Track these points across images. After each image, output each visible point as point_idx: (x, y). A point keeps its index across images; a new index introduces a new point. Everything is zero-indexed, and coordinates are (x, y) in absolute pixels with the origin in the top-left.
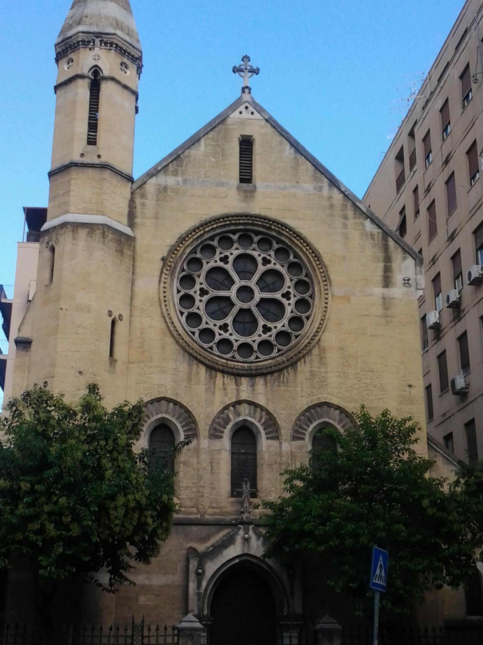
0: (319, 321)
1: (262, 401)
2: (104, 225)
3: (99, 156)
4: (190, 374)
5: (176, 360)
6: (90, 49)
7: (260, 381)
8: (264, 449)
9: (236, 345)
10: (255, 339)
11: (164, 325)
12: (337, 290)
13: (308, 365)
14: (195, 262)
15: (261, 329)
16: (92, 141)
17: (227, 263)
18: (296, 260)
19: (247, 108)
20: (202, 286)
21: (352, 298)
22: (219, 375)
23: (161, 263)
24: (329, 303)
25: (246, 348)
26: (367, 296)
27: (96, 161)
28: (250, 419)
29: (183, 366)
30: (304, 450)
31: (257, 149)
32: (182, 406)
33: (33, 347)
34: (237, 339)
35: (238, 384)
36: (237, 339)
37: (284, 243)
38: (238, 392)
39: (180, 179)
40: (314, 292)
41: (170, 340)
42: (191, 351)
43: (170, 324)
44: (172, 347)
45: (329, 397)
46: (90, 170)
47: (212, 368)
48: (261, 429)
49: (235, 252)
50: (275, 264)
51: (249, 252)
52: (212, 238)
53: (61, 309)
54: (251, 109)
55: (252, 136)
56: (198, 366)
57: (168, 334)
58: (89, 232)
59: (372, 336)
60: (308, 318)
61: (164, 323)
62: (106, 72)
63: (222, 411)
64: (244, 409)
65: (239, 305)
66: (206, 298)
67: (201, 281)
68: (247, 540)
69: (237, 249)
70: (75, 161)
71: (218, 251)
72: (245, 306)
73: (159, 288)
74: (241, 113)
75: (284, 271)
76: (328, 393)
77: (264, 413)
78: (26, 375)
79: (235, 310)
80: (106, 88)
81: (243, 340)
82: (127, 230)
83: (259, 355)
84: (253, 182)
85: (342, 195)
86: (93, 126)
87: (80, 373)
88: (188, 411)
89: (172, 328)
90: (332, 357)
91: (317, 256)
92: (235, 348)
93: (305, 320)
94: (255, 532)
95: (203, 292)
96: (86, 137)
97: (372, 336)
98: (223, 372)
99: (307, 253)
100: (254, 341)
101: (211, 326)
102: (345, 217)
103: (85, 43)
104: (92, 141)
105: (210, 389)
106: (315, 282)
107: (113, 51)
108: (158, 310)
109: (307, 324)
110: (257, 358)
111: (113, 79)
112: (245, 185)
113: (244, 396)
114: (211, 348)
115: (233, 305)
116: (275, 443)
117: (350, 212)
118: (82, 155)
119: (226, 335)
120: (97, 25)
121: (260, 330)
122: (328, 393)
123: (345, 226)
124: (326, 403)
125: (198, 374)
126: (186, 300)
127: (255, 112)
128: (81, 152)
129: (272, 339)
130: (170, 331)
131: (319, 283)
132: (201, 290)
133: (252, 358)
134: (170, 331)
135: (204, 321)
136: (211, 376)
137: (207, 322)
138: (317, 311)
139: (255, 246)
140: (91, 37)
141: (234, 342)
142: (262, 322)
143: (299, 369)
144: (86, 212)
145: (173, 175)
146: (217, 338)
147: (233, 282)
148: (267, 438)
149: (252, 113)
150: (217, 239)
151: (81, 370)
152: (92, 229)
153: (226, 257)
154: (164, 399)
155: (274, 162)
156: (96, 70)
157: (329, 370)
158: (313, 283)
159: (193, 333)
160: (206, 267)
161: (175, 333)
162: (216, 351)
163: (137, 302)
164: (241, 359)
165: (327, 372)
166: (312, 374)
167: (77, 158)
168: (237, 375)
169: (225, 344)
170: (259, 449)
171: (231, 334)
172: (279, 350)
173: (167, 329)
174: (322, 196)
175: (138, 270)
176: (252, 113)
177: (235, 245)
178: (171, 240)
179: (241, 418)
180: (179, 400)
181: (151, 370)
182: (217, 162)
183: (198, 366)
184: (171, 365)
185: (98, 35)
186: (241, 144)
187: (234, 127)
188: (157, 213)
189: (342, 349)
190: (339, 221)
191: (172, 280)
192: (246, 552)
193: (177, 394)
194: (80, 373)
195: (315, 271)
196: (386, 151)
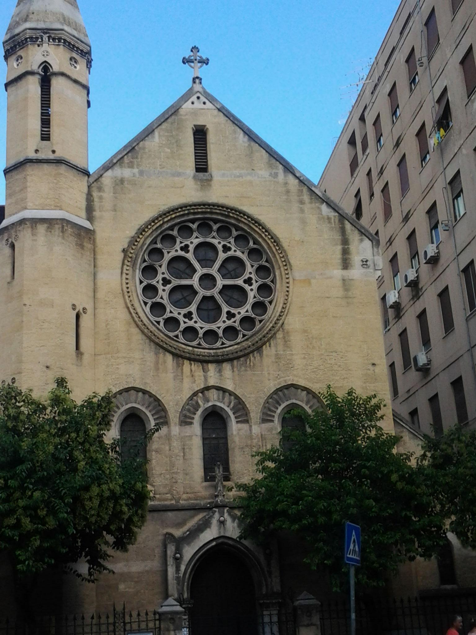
0: (281, 305)
1: (229, 386)
3: (54, 152)
4: (157, 363)
8: (235, 433)
10: (220, 325)
12: (297, 274)
13: (273, 348)
14: (156, 253)
16: (46, 137)
18: (255, 246)
19: (198, 98)
20: (164, 276)
21: (313, 281)
22: (186, 363)
23: (122, 255)
25: (211, 335)
26: (327, 278)
27: (51, 156)
28: (219, 404)
30: (274, 432)
31: (211, 138)
32: (151, 395)
34: (202, 326)
36: (202, 326)
37: (243, 229)
40: (275, 276)
41: (135, 330)
42: (157, 340)
43: (134, 315)
44: (137, 336)
45: (296, 379)
46: (45, 166)
47: (178, 356)
48: (231, 413)
49: (195, 241)
50: (235, 251)
51: (209, 240)
52: (171, 228)
54: (203, 99)
55: (205, 126)
57: (133, 325)
59: (334, 317)
60: (270, 302)
62: (56, 68)
63: (191, 398)
64: (213, 395)
67: (163, 270)
68: (222, 523)
69: (197, 237)
71: (178, 241)
72: (208, 293)
73: (122, 280)
74: (193, 103)
75: (244, 257)
76: (295, 376)
77: (232, 397)
79: (198, 298)
80: (57, 84)
83: (225, 341)
85: (297, 181)
86: (46, 122)
87: (47, 367)
88: (157, 400)
89: (136, 319)
90: (297, 340)
91: (277, 242)
92: (201, 335)
94: (230, 514)
97: (334, 317)
98: (189, 359)
99: (266, 238)
100: (219, 328)
101: (175, 315)
102: (302, 202)
104: (46, 137)
105: (179, 377)
106: (276, 267)
107: (62, 47)
108: (122, 301)
109: (270, 309)
110: (223, 344)
111: (63, 74)
112: (201, 175)
114: (177, 336)
115: (196, 293)
116: (245, 426)
117: (306, 197)
118: (37, 151)
119: (191, 323)
121: (224, 316)
122: (295, 376)
123: (302, 211)
125: (165, 362)
126: (150, 290)
128: (35, 148)
130: (135, 322)
133: (218, 344)
134: (135, 322)
135: (168, 310)
137: (172, 311)
138: (279, 295)
139: (214, 234)
140: (39, 34)
141: (199, 329)
142: (225, 309)
145: (129, 167)
147: (195, 271)
148: (237, 422)
149: (204, 103)
150: (176, 229)
151: (48, 364)
153: (187, 246)
155: (229, 151)
156: (46, 66)
159: (158, 323)
162: (181, 339)
163: (99, 295)
164: (207, 346)
165: (292, 355)
167: (32, 155)
168: (204, 361)
169: (191, 332)
171: (196, 322)
172: (244, 336)
174: (278, 183)
176: (204, 103)
177: (195, 234)
179: (210, 404)
183: (165, 354)
184: (137, 355)
185: (46, 31)
188: (115, 206)
190: (295, 206)
191: (134, 271)
192: (222, 534)
194: (47, 367)
195: (275, 256)
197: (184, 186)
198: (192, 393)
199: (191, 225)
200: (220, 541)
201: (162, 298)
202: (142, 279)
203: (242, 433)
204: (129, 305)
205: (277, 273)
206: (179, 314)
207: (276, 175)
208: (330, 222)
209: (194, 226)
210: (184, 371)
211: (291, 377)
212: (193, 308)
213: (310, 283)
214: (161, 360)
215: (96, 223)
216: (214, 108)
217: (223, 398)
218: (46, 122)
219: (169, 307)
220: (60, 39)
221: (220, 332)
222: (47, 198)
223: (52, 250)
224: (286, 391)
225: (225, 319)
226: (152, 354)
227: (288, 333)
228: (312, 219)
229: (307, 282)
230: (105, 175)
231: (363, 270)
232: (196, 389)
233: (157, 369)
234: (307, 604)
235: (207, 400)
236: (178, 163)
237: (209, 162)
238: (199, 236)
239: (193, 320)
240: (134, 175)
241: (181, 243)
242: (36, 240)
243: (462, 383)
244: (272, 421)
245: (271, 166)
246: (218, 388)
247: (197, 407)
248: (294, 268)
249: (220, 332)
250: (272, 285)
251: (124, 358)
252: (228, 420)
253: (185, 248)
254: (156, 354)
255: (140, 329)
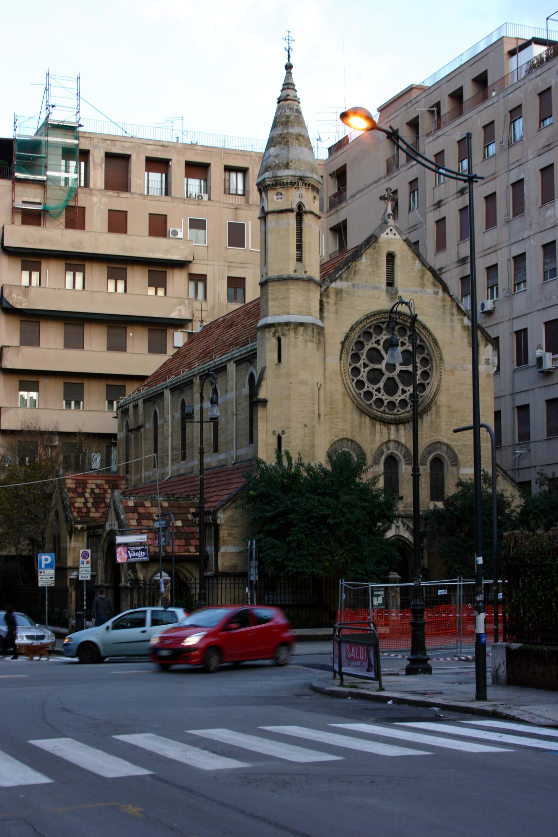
0: (436, 387)
2: (313, 324)
3: (305, 272)
4: (360, 423)
5: (352, 413)
6: (295, 188)
7: (401, 427)
8: (404, 471)
9: (386, 402)
11: (344, 390)
12: (447, 366)
13: (429, 417)
14: (360, 344)
15: (367, 363)
16: (300, 259)
17: (379, 344)
18: (421, 344)
19: (391, 230)
20: (364, 361)
21: (456, 372)
22: (378, 423)
24: (443, 375)
25: (392, 404)
26: (464, 370)
27: (304, 276)
28: (395, 452)
29: (356, 417)
30: (426, 472)
31: (398, 262)
32: (356, 444)
33: (269, 405)
34: (386, 398)
35: (389, 429)
36: (386, 398)
38: (389, 434)
39: (350, 284)
40: (432, 366)
41: (348, 400)
42: (361, 408)
43: (348, 389)
44: (349, 404)
45: (441, 438)
46: (301, 283)
47: (374, 418)
48: (402, 458)
49: (384, 337)
50: (408, 346)
52: (370, 327)
53: (291, 383)
54: (394, 231)
55: (394, 252)
56: (365, 417)
57: (347, 396)
58: (304, 329)
59: (467, 398)
60: (428, 384)
61: (344, 388)
62: (307, 208)
63: (379, 447)
65: (387, 375)
66: (367, 369)
67: (364, 358)
68: (398, 527)
69: (385, 335)
70: (291, 276)
71: (374, 336)
72: (391, 375)
73: (340, 364)
74: (387, 234)
76: (440, 436)
77: (403, 448)
78: (265, 424)
79: (384, 378)
80: (307, 219)
81: (390, 398)
82: (319, 323)
83: (400, 409)
84: (395, 286)
85: (450, 298)
86: (299, 247)
87: (305, 426)
88: (360, 447)
89: (349, 392)
90: (443, 411)
91: (436, 342)
92: (385, 404)
93: (426, 385)
94: (402, 522)
95: (365, 365)
96: (296, 257)
97: (467, 398)
98: (380, 421)
99: (429, 339)
100: (396, 400)
101: (370, 389)
102: (452, 314)
103: (293, 184)
104: (300, 259)
105: (373, 433)
106: (434, 360)
107: (310, 190)
108: (340, 379)
109: (428, 389)
110: (398, 411)
111: (312, 213)
112: (390, 288)
113: (392, 437)
114: (371, 404)
115: (383, 374)
117: (455, 311)
118: (295, 271)
119: (380, 396)
120: (300, 170)
121: (400, 392)
122: (440, 436)
123: (452, 321)
124: (439, 442)
125: (365, 422)
126: (356, 371)
127: (397, 234)
128: (294, 269)
129: (407, 398)
130: (349, 394)
131: (436, 361)
132: (364, 364)
133: (395, 411)
134: (349, 394)
135: (366, 386)
136: (373, 424)
137: (368, 387)
138: (434, 380)
140: (296, 180)
141: (384, 400)
142: (401, 387)
143: (424, 419)
144: (300, 313)
145: (346, 281)
146: (375, 398)
149: (395, 234)
150: (373, 327)
151: (306, 424)
152: (305, 327)
153: (379, 341)
154: (346, 439)
155: (409, 272)
156: (300, 206)
157: (441, 420)
158: (432, 360)
159: (360, 394)
160: (367, 348)
161: (351, 395)
162: (374, 406)
163: (327, 374)
164: (389, 412)
165: (440, 422)
166: (432, 422)
167: (292, 274)
168: (386, 423)
169: (380, 401)
170: (400, 471)
171: (383, 395)
173: (346, 392)
174: (438, 298)
175: (327, 351)
176: (395, 234)
177: (384, 332)
178: (346, 330)
179: (390, 451)
180: (355, 440)
181: (338, 420)
182: (373, 271)
183: (365, 417)
184: (349, 417)
185: (301, 178)
186: (387, 257)
187: (383, 244)
188: (337, 309)
189: (449, 406)
190: (448, 317)
191: (347, 357)
192: (397, 533)
193: (354, 436)
194: (305, 426)
195: (433, 352)
196: (455, 181)
197: (379, 298)
198: (380, 444)
199: (382, 325)
200: (397, 537)
201: (363, 377)
202: (351, 363)
203: (408, 471)
204: (345, 382)
205: (434, 365)
206: (373, 389)
207: (436, 293)
208: (468, 330)
209: (384, 326)
210: (377, 428)
211: (439, 437)
212: (381, 385)
213: (454, 373)
214: (363, 421)
215: (325, 322)
216: (401, 238)
217: (398, 447)
218: (299, 247)
219: (367, 384)
220: (309, 185)
221: (397, 403)
222: (302, 307)
223: (306, 345)
224: (435, 445)
225: (400, 394)
226: (358, 416)
227: (439, 407)
228: (458, 327)
229: (452, 371)
230: (331, 286)
231: (486, 366)
232: (383, 442)
233: (360, 427)
234: (322, 629)
235: (388, 449)
236: (377, 280)
237: (395, 280)
238: (387, 333)
239: (381, 394)
240: (349, 288)
241: (375, 338)
242: (297, 338)
243: (445, 222)
244: (426, 465)
245: (434, 285)
246: (396, 442)
247: (382, 453)
248: (445, 362)
249: (397, 403)
250: (430, 373)
251: (341, 418)
252: (400, 462)
253: (378, 342)
254: (360, 416)
255: (351, 399)
